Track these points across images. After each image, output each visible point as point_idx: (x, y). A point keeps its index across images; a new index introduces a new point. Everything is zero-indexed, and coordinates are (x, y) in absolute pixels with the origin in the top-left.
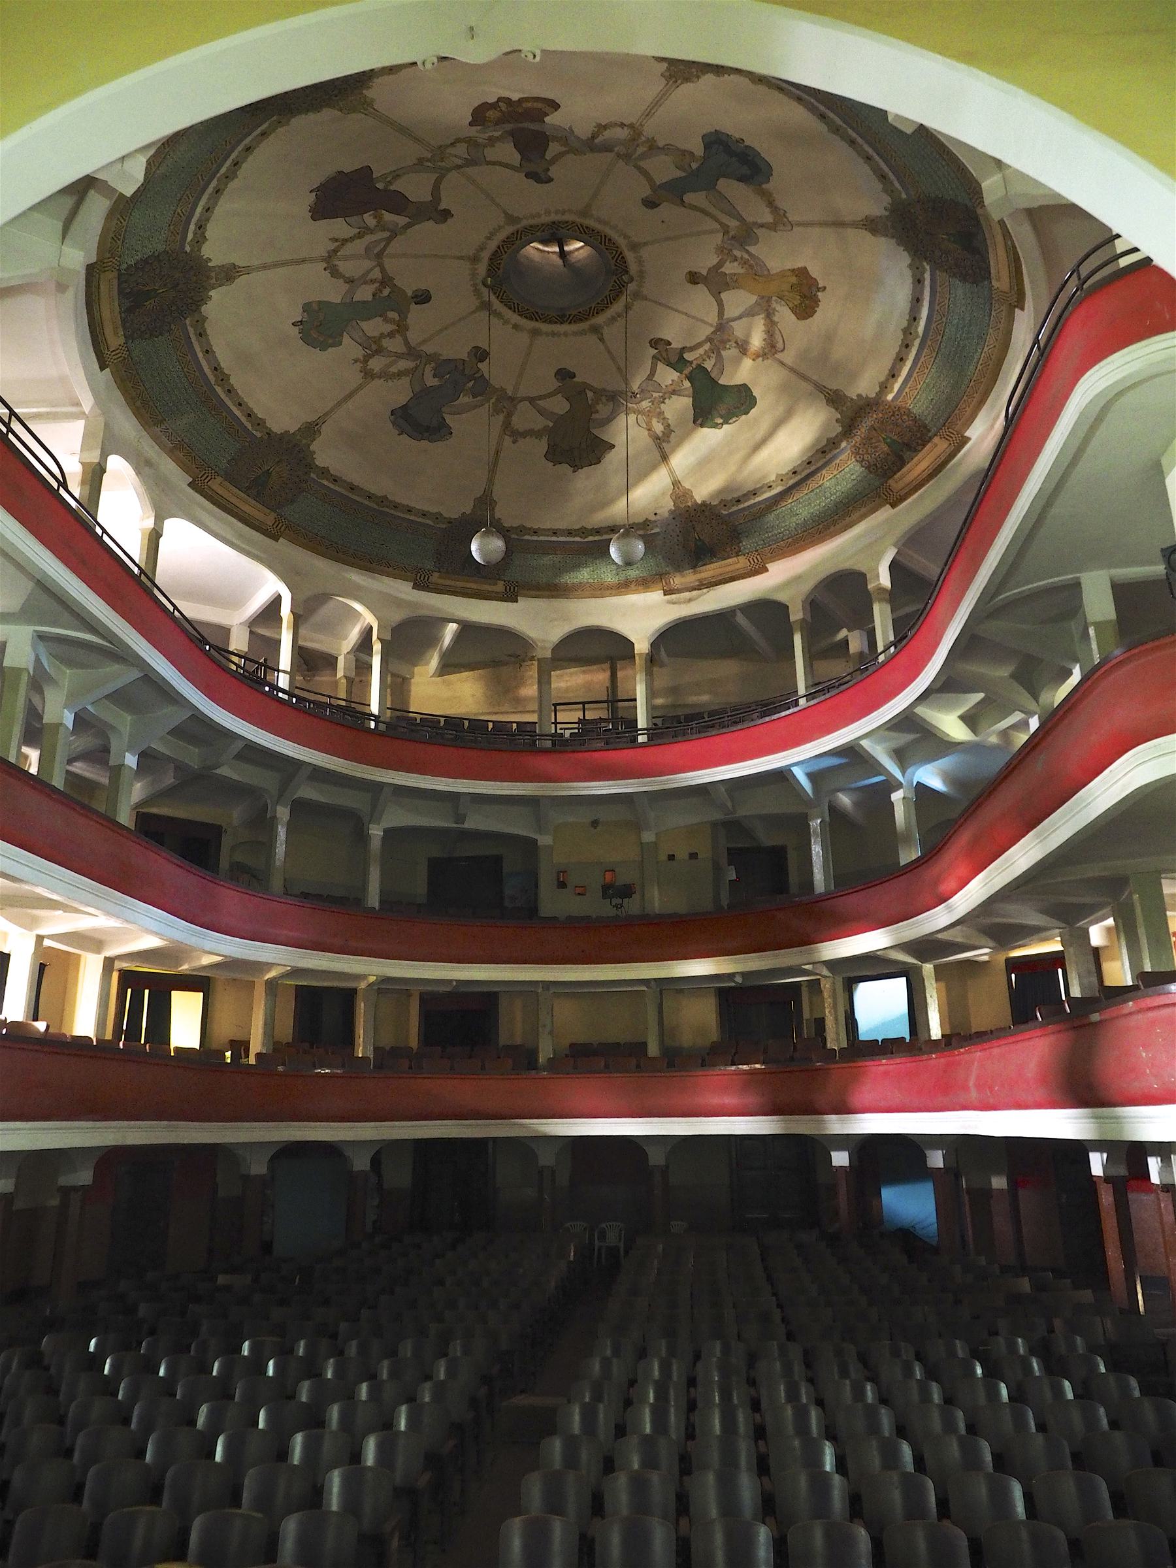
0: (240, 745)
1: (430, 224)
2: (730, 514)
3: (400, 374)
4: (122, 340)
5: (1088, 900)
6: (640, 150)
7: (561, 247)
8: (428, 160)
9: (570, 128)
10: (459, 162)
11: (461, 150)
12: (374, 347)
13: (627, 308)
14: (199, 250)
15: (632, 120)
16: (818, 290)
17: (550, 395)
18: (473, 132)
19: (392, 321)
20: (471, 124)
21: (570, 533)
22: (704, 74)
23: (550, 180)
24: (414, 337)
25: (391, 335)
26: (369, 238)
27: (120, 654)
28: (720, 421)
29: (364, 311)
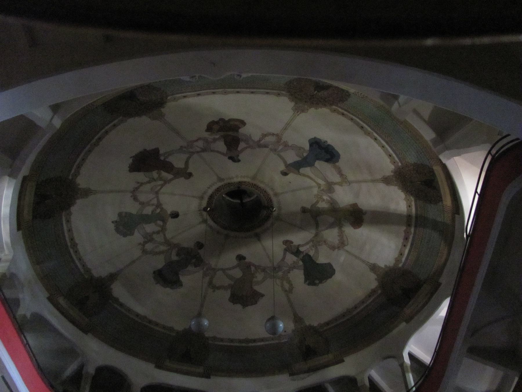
1: (182, 179)
4: (31, 217)
6: (281, 147)
7: (241, 200)
8: (185, 147)
9: (250, 135)
10: (199, 149)
11: (200, 144)
12: (149, 238)
17: (234, 268)
18: (206, 135)
21: (240, 341)
22: (310, 108)
24: (169, 236)
25: (158, 233)
26: (153, 184)
28: (317, 282)
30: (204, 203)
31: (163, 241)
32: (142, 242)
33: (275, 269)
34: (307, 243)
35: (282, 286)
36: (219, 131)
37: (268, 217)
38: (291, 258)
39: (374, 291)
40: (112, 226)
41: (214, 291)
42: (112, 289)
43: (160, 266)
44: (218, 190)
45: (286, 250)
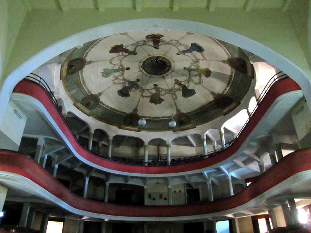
0: (81, 163)
2: (189, 115)
3: (121, 83)
4: (66, 74)
5: (277, 204)
11: (142, 43)
12: (116, 78)
13: (171, 73)
14: (85, 58)
15: (178, 40)
16: (211, 72)
19: (121, 73)
20: (145, 38)
21: (153, 118)
23: (159, 49)
25: (120, 76)
27: (62, 143)
28: (188, 96)
29: (116, 71)
30: (141, 64)
31: (123, 79)
32: (113, 80)
33: (170, 90)
34: (185, 81)
35: (172, 97)
36: (151, 38)
37: (169, 70)
38: (177, 86)
39: (211, 102)
40: (101, 74)
41: (143, 98)
42: (100, 99)
43: (120, 89)
44: (148, 59)
45: (175, 83)
